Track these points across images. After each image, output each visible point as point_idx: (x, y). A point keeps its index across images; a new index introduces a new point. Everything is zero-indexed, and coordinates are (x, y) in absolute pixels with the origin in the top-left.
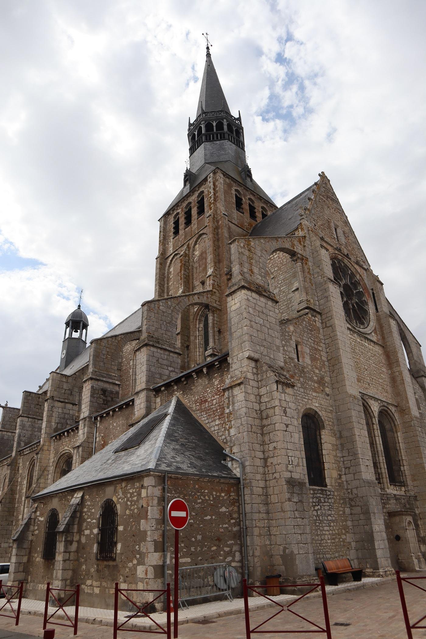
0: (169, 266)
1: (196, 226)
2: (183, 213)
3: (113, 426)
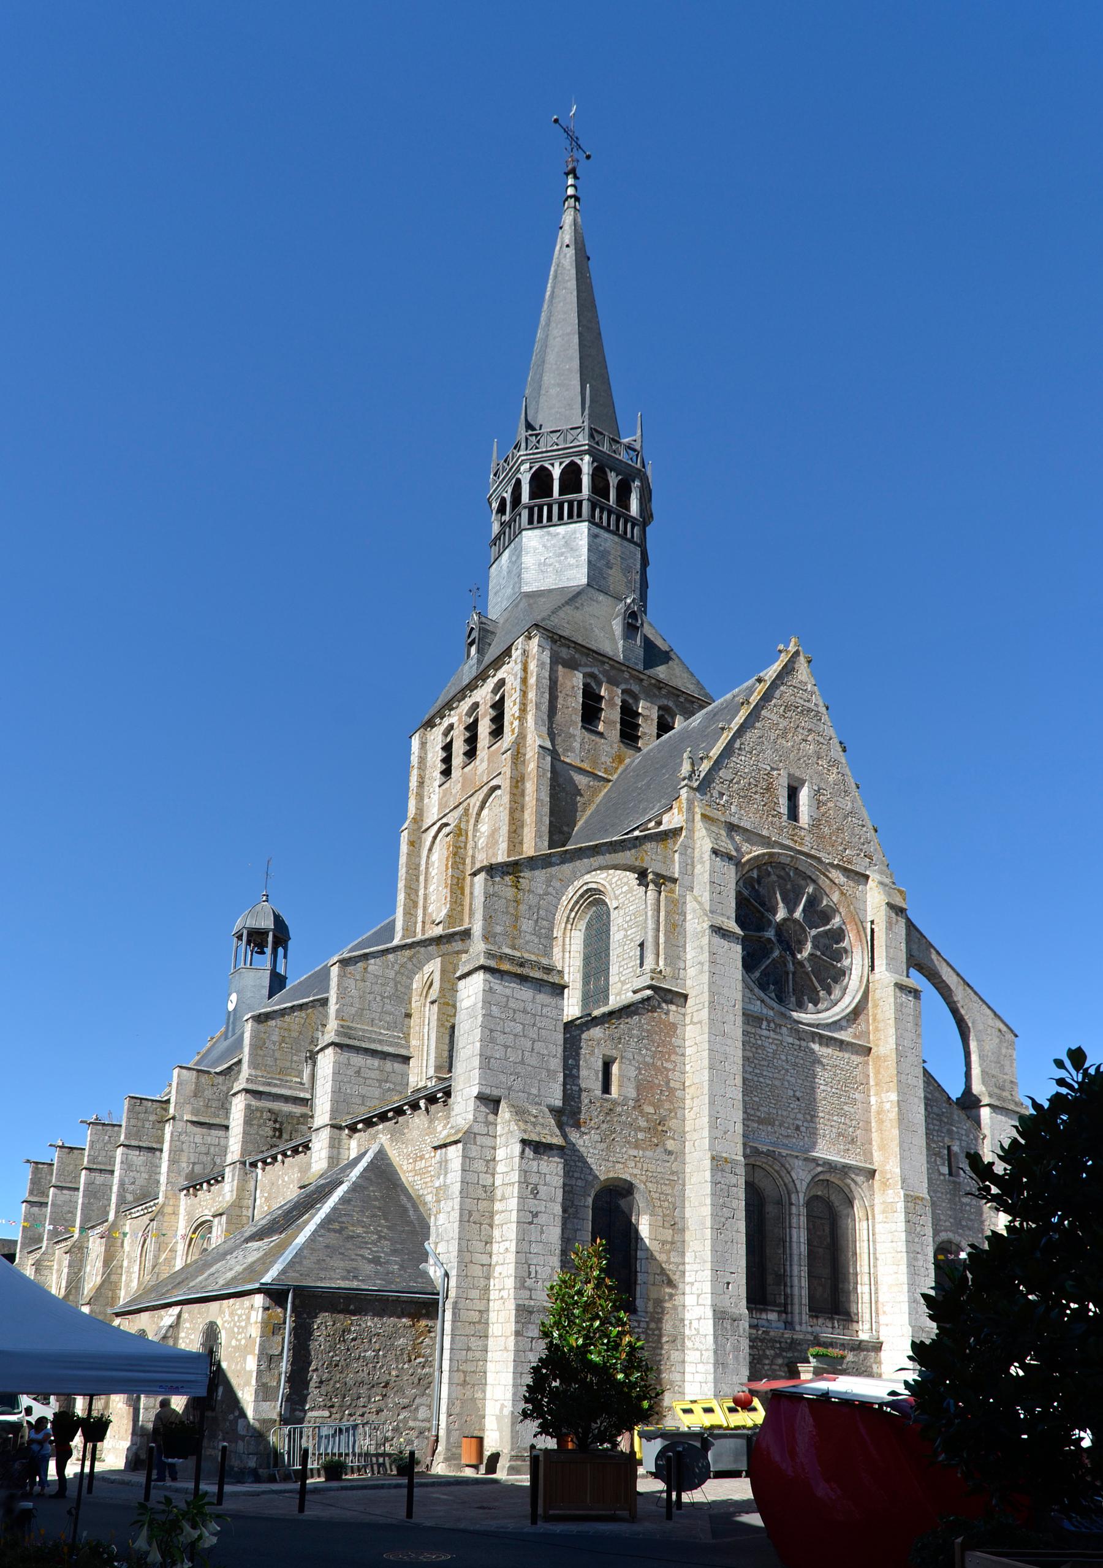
0: (430, 850)
1: (485, 765)
2: (462, 727)
3: (283, 1181)
